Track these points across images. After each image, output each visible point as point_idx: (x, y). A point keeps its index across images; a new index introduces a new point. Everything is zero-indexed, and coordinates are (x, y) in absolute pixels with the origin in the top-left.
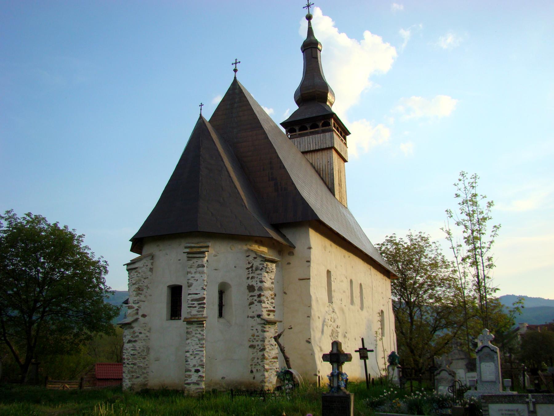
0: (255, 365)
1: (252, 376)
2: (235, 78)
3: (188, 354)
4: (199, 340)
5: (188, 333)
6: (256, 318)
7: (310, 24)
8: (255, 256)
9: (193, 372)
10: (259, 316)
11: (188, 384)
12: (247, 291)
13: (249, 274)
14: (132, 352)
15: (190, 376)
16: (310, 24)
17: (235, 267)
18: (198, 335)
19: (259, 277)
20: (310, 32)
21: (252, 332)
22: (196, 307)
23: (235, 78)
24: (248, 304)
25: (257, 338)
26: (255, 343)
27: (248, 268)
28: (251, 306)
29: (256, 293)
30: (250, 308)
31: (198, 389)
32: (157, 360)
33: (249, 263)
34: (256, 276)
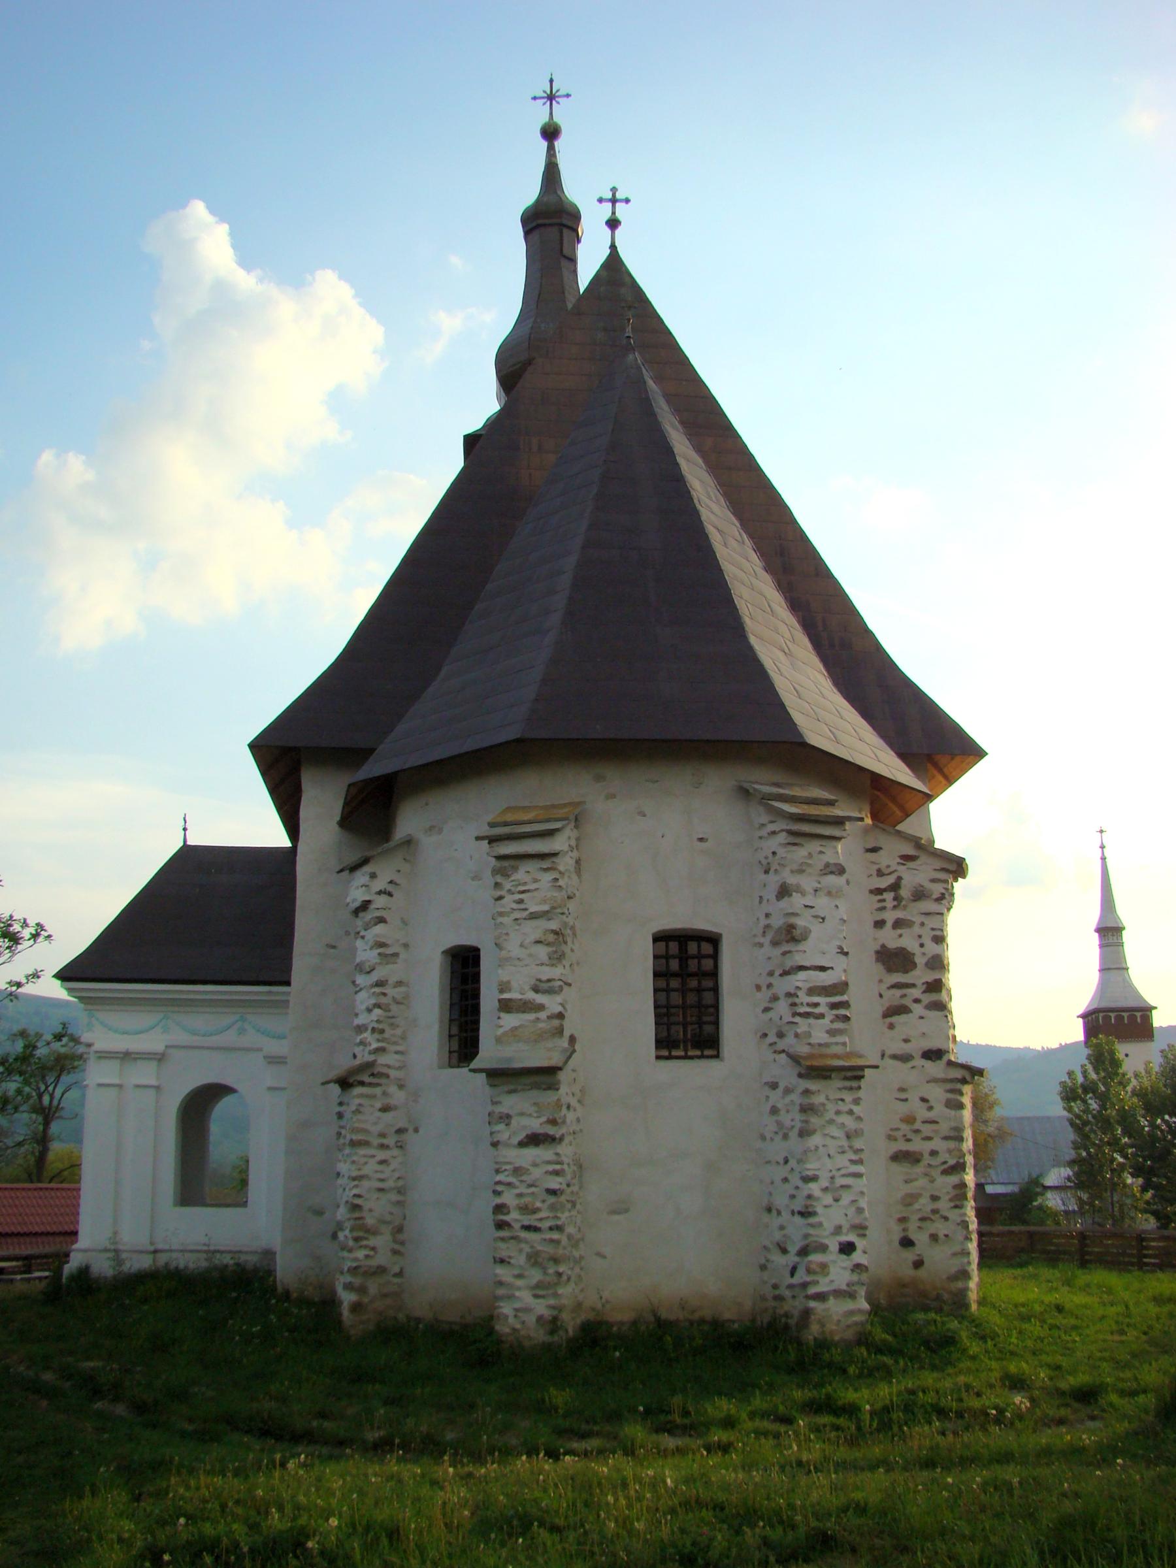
0: (922, 1219)
1: (909, 1255)
2: (613, 247)
4: (848, 1137)
6: (919, 1062)
7: (551, 150)
8: (910, 851)
11: (821, 1297)
12: (880, 968)
16: (551, 150)
18: (845, 1119)
19: (931, 922)
21: (903, 1109)
22: (822, 1016)
23: (613, 247)
25: (927, 1129)
26: (916, 1145)
27: (878, 891)
28: (894, 1019)
29: (920, 976)
30: (891, 1026)
31: (851, 1313)
32: (620, 1208)
33: (880, 873)
34: (918, 919)
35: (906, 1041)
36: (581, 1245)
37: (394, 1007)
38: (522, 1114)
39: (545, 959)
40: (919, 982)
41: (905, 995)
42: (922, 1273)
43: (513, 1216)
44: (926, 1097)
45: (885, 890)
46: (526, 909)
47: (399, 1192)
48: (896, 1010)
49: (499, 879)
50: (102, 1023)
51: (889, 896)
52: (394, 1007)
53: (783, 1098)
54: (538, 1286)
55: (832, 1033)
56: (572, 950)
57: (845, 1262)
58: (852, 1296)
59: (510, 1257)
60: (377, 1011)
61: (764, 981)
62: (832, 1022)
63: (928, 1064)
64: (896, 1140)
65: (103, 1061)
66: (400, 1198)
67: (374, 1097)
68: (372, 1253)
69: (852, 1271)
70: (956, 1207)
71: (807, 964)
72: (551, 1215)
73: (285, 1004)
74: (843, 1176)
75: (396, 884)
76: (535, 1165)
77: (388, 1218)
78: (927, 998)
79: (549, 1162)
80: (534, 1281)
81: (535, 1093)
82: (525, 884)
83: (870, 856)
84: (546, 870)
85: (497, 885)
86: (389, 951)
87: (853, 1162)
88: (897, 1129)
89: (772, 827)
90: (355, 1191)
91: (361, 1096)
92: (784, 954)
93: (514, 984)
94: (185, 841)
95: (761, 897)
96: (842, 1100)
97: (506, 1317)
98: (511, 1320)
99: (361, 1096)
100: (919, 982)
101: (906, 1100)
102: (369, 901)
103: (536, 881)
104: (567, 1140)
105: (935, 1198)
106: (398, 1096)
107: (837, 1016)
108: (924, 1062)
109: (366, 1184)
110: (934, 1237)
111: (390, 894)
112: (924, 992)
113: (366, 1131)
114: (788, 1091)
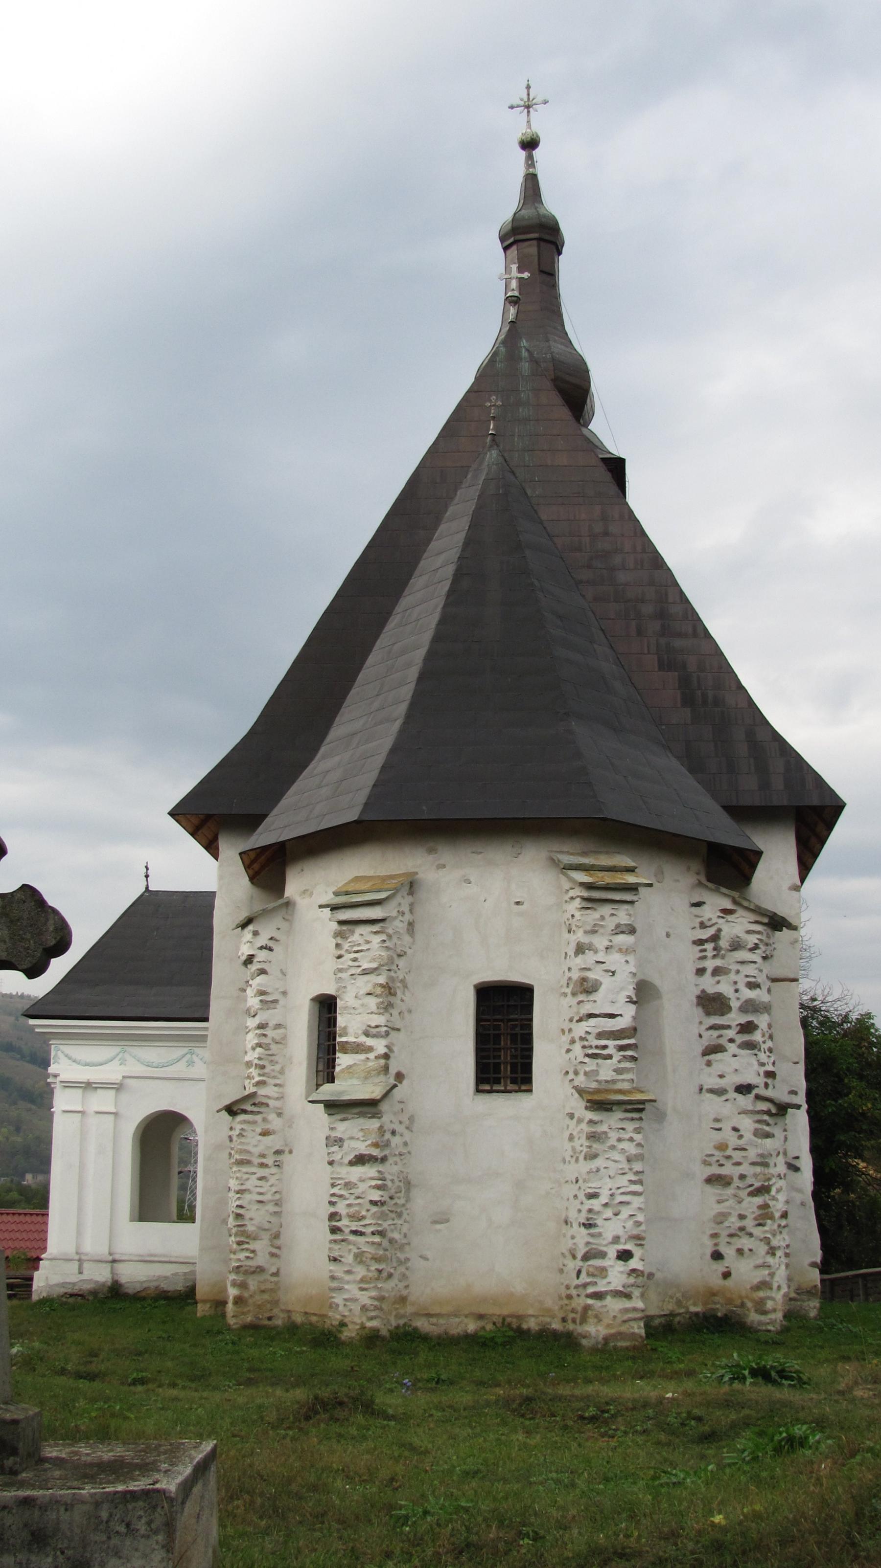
0: (731, 1235)
3: (596, 1204)
4: (629, 1160)
5: (593, 1137)
6: (732, 1095)
7: (530, 161)
9: (610, 1261)
10: (744, 1089)
12: (699, 1012)
13: (704, 958)
14: (376, 1195)
15: (602, 1272)
16: (530, 161)
17: (668, 935)
20: (531, 187)
21: (717, 1137)
22: (610, 1057)
24: (700, 1050)
25: (737, 1156)
26: (727, 1170)
27: (700, 942)
28: (712, 1057)
29: (735, 1018)
30: (709, 1064)
31: (626, 1310)
32: (441, 1219)
33: (703, 926)
34: (734, 967)
35: (721, 1076)
36: (407, 1248)
37: (273, 1047)
38: (352, 1138)
39: (374, 1008)
40: (734, 1024)
41: (720, 1036)
42: (729, 1283)
43: (344, 1223)
44: (737, 1126)
45: (706, 941)
46: (359, 966)
47: (276, 1204)
48: (715, 1049)
49: (339, 941)
50: (66, 1056)
51: (709, 946)
52: (273, 1047)
53: (577, 1126)
54: (362, 1280)
55: (618, 1071)
56: (402, 1000)
57: (620, 1266)
58: (628, 1296)
59: (341, 1256)
60: (259, 1050)
61: (566, 1026)
62: (619, 1062)
63: (740, 1097)
64: (710, 1165)
65: (68, 1090)
66: (277, 1209)
67: (255, 1122)
68: (252, 1255)
69: (629, 1275)
70: (760, 1225)
71: (597, 1012)
72: (373, 1222)
73: (203, 1039)
74: (623, 1193)
75: (277, 940)
76: (362, 1180)
77: (267, 1226)
78: (740, 1038)
79: (372, 1179)
80: (359, 1277)
81: (361, 1121)
82: (359, 945)
83: (695, 910)
84: (376, 933)
85: (338, 946)
86: (269, 998)
87: (632, 1182)
88: (712, 1155)
89: (572, 893)
90: (238, 1203)
91: (245, 1122)
92: (579, 1003)
93: (350, 1030)
94: (147, 888)
95: (566, 953)
96: (623, 1129)
97: (338, 1305)
98: (341, 1308)
99: (245, 1122)
100: (734, 1024)
101: (719, 1129)
102: (253, 955)
103: (368, 942)
104: (391, 1160)
105: (742, 1217)
106: (275, 1122)
107: (624, 1056)
108: (736, 1095)
109: (247, 1197)
110: (740, 1252)
111: (271, 949)
112: (738, 1033)
113: (248, 1152)
114: (580, 1121)
